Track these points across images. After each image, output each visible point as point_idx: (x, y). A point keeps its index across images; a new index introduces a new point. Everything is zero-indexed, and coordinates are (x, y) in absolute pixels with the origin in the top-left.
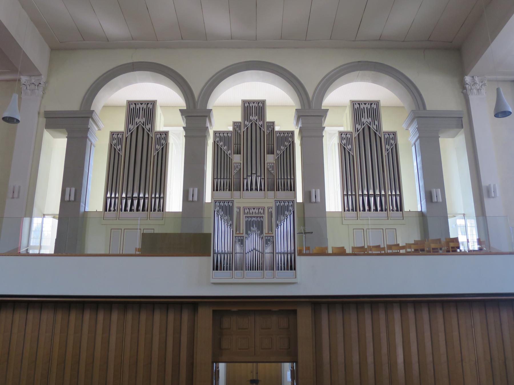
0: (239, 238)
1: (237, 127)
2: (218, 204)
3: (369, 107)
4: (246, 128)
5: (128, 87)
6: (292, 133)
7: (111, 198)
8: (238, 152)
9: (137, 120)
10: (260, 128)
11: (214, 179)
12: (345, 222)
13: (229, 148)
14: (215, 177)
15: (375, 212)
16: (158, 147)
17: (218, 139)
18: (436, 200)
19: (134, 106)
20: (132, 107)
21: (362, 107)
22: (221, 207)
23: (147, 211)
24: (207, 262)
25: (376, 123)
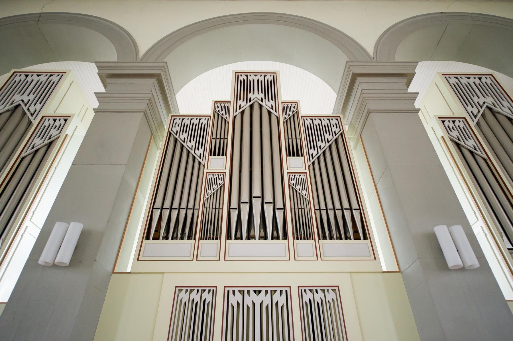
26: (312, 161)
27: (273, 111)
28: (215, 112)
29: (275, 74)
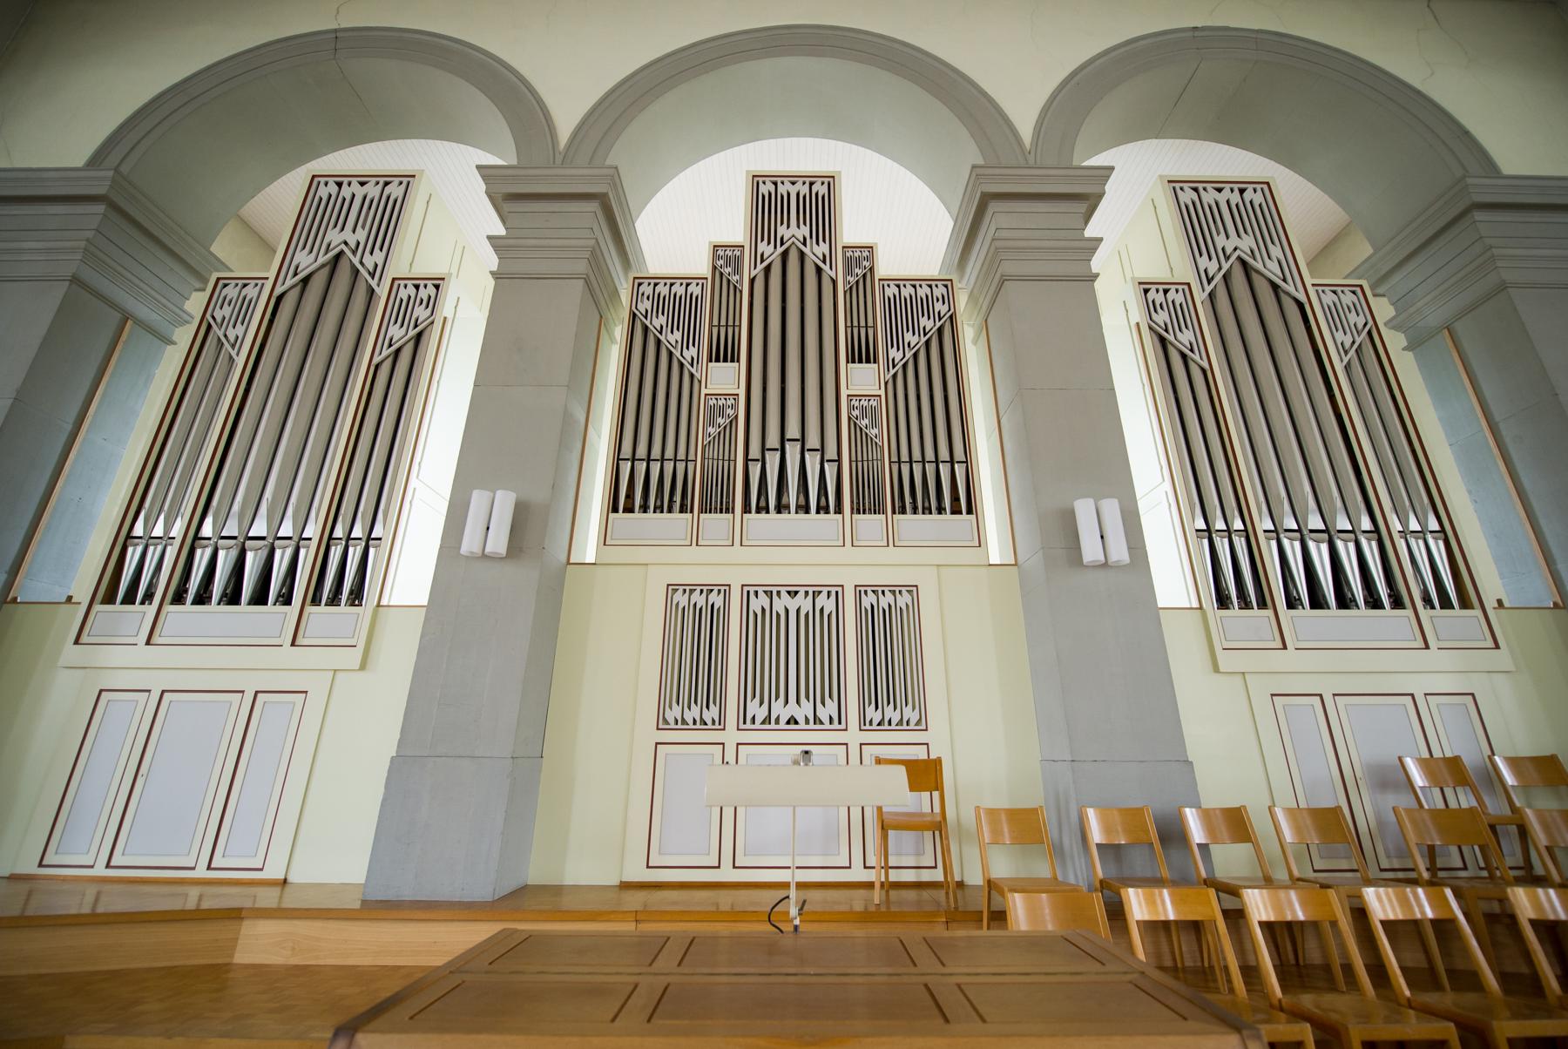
26: (892, 372)
27: (826, 268)
28: (714, 268)
29: (742, 726)
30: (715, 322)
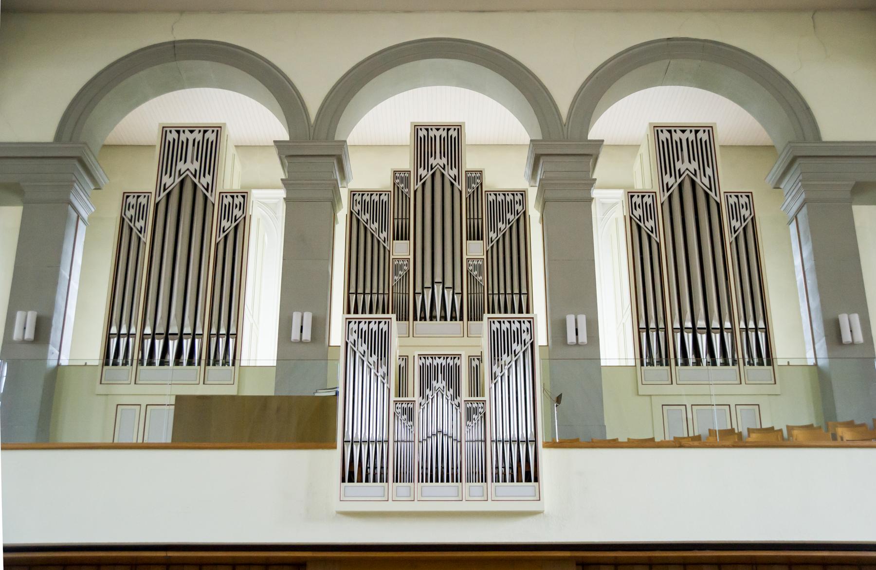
0: (405, 406)
1: (402, 182)
2: (355, 327)
3: (692, 137)
4: (420, 184)
5: (163, 96)
6: (523, 193)
7: (119, 335)
8: (401, 235)
9: (181, 166)
10: (452, 184)
11: (349, 293)
12: (643, 390)
13: (383, 227)
14: (353, 290)
15: (711, 367)
16: (225, 224)
17: (359, 207)
18: (850, 340)
19: (175, 135)
20: (170, 137)
21: (676, 137)
22: (361, 333)
23: (199, 364)
24: (330, 461)
25: (709, 171)
30: (396, 217)
